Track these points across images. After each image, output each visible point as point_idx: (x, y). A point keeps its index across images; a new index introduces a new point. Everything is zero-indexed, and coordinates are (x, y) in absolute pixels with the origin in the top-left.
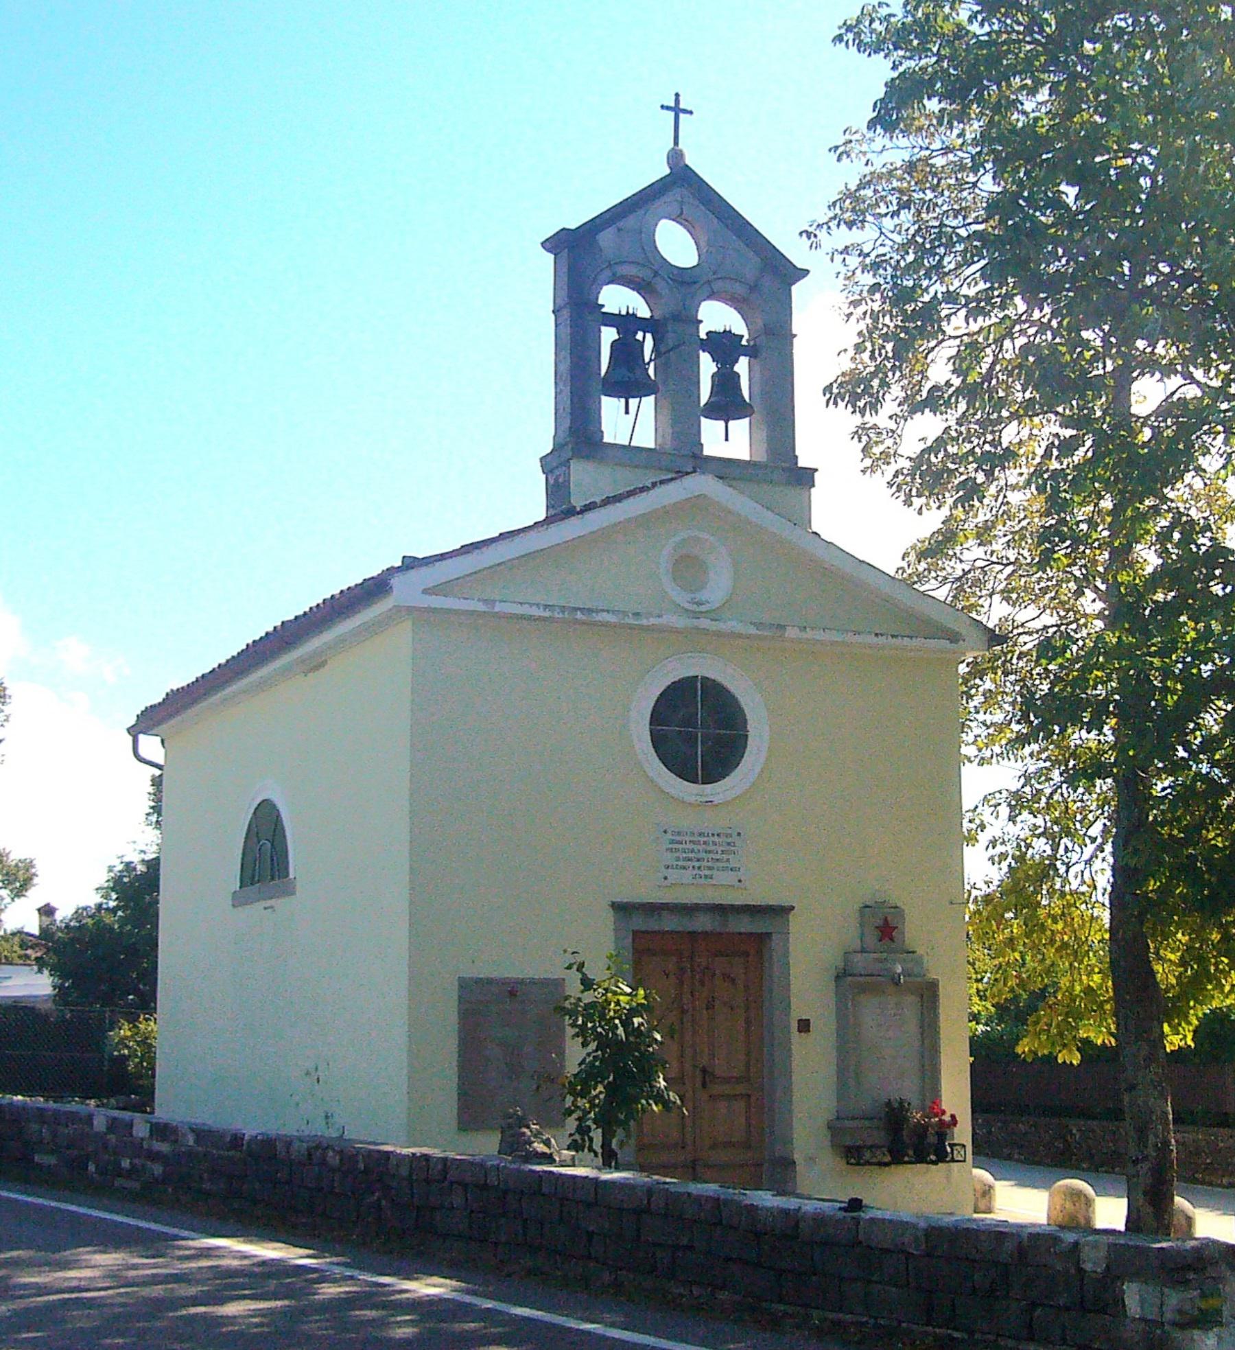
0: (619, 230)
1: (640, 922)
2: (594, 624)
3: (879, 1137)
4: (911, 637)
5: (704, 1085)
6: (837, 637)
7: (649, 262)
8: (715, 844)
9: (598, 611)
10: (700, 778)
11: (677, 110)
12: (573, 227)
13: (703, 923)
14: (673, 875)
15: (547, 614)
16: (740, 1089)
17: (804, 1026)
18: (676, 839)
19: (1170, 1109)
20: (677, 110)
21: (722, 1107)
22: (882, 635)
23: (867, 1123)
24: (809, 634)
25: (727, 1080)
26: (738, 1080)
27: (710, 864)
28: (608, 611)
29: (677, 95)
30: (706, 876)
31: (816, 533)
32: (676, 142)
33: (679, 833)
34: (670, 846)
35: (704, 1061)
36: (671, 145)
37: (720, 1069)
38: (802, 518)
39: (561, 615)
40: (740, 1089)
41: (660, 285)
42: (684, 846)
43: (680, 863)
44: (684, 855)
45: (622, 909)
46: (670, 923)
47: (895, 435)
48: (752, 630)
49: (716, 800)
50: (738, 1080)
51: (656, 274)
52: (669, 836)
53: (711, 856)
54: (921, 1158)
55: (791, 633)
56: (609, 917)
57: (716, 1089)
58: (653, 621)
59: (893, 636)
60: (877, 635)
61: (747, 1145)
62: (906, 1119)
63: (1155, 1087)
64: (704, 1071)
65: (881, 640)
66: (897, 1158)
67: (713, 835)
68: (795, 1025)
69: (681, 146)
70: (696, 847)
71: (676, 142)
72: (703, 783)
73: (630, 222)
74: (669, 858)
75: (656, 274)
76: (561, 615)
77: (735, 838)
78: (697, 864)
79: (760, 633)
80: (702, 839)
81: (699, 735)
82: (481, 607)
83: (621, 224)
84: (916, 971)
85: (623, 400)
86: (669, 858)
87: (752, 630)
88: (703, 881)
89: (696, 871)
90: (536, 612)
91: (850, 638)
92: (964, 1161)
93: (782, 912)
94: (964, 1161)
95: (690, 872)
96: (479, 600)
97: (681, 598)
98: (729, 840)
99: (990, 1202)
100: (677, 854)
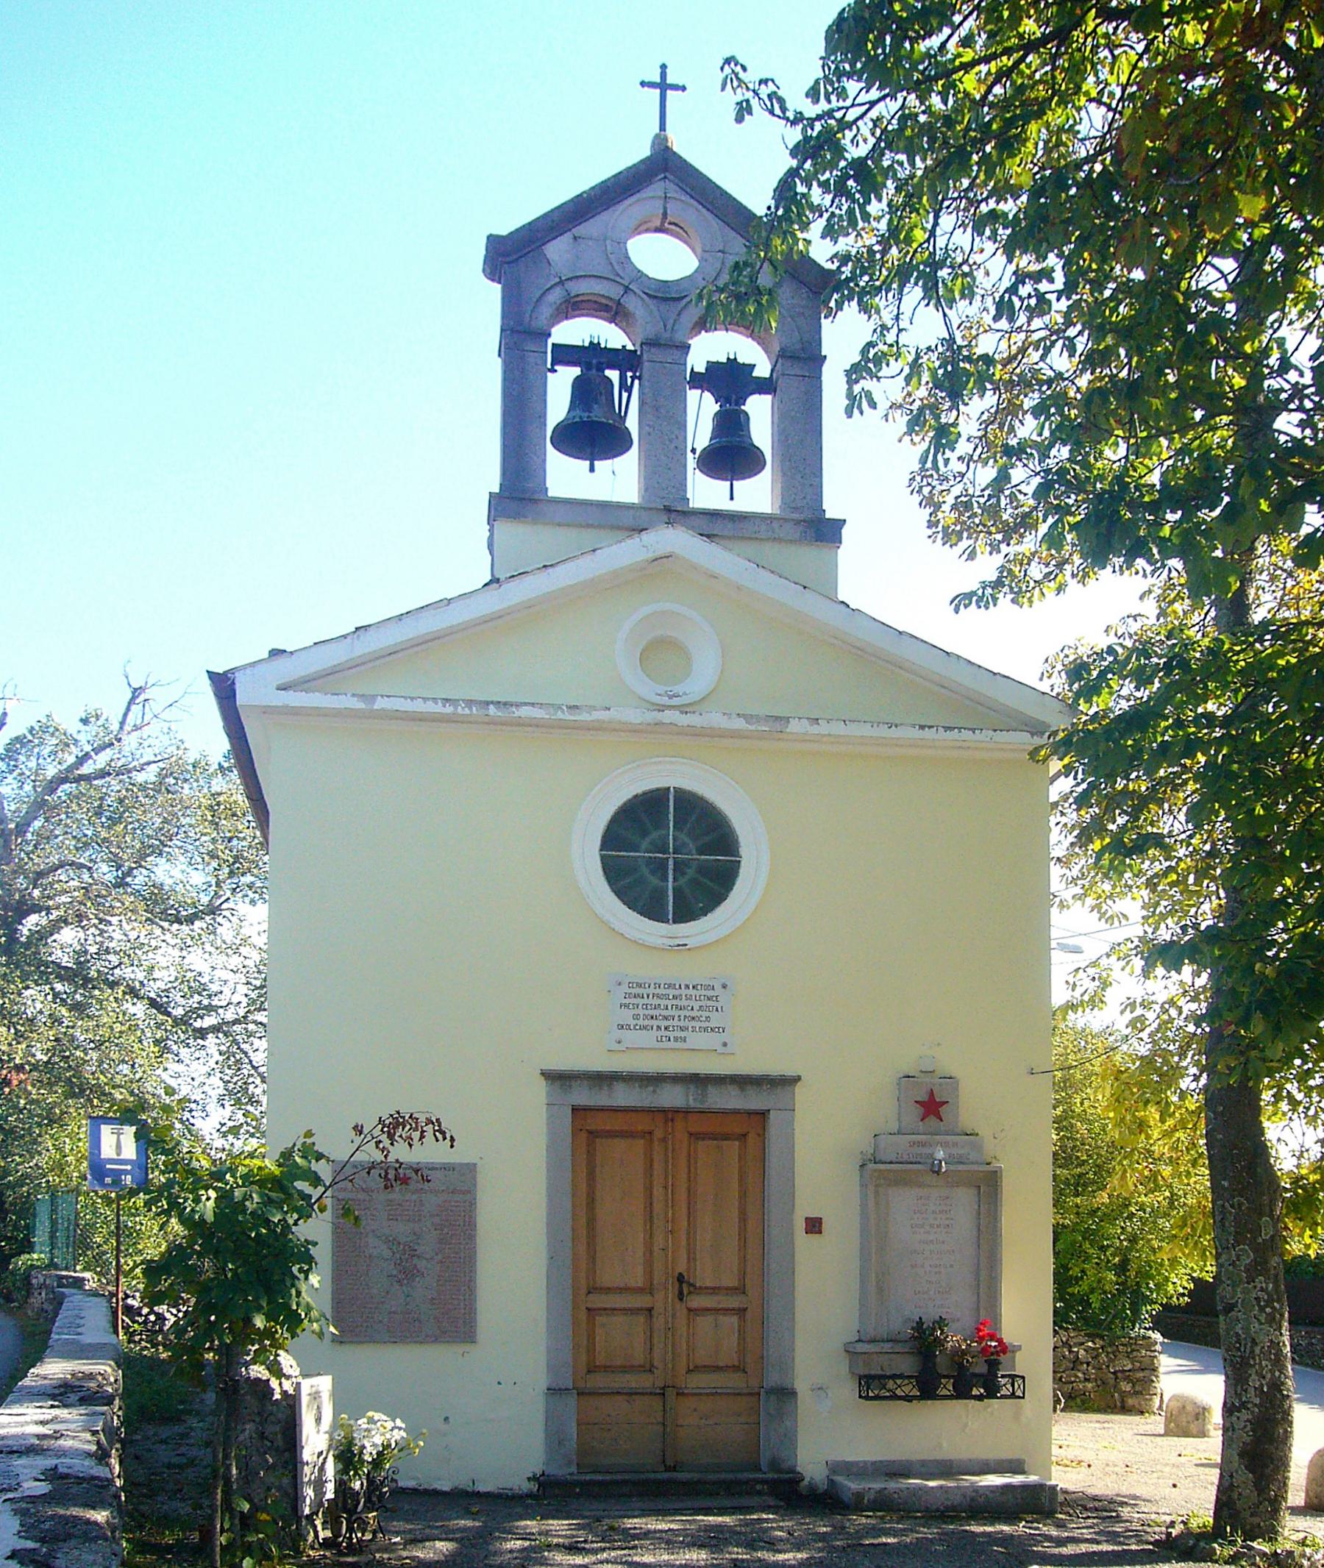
0: (575, 238)
1: (583, 1097)
2: (520, 723)
3: (907, 1365)
4: (973, 730)
5: (681, 1296)
6: (866, 731)
7: (618, 275)
8: (689, 998)
9: (518, 705)
10: (670, 917)
11: (663, 86)
12: (504, 233)
13: (672, 1097)
14: (632, 1038)
15: (449, 709)
16: (734, 1302)
17: (814, 1226)
18: (636, 993)
19: (1286, 1339)
20: (663, 86)
21: (705, 1323)
22: (930, 727)
23: (887, 1347)
24: (823, 728)
25: (715, 1290)
26: (640, 1290)
27: (682, 1024)
28: (533, 705)
29: (664, 67)
30: (676, 1039)
31: (843, 602)
32: (663, 126)
33: (639, 985)
34: (627, 1001)
35: (682, 1267)
36: (657, 130)
37: (704, 1277)
38: (825, 586)
39: (467, 711)
40: (734, 1302)
41: (631, 303)
42: (645, 1001)
43: (641, 1022)
44: (647, 1012)
45: (558, 1078)
46: (623, 1097)
47: (965, 480)
48: (740, 724)
49: (692, 943)
50: (640, 1290)
51: (627, 289)
52: (625, 988)
53: (683, 1013)
54: (962, 1392)
55: (795, 727)
56: (539, 1091)
57: (697, 1301)
58: (597, 715)
59: (947, 729)
60: (922, 727)
61: (739, 1368)
62: (940, 1343)
63: (1262, 1309)
64: (680, 1279)
65: (928, 733)
66: (928, 1391)
67: (687, 987)
68: (800, 1225)
69: (670, 132)
70: (663, 1002)
71: (663, 126)
72: (674, 922)
73: (590, 228)
74: (626, 1016)
75: (627, 289)
76: (467, 711)
77: (719, 990)
78: (664, 1024)
79: (751, 728)
80: (671, 992)
81: (671, 862)
82: (359, 705)
83: (580, 230)
84: (973, 1157)
85: (588, 462)
86: (626, 1016)
87: (740, 724)
88: (672, 1044)
89: (663, 1033)
90: (438, 708)
91: (884, 732)
92: (1023, 1398)
93: (787, 1082)
94: (1023, 1398)
95: (654, 1033)
96: (354, 695)
97: (649, 690)
98: (710, 993)
99: (1204, 1425)
100: (636, 1012)
